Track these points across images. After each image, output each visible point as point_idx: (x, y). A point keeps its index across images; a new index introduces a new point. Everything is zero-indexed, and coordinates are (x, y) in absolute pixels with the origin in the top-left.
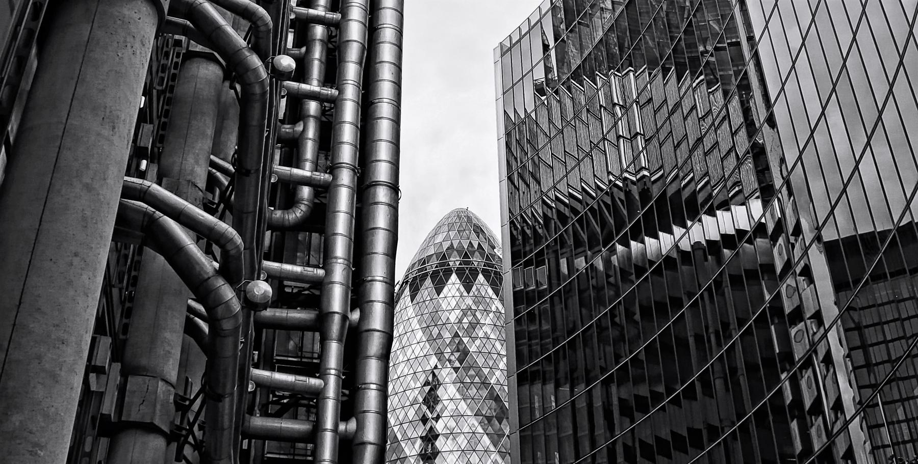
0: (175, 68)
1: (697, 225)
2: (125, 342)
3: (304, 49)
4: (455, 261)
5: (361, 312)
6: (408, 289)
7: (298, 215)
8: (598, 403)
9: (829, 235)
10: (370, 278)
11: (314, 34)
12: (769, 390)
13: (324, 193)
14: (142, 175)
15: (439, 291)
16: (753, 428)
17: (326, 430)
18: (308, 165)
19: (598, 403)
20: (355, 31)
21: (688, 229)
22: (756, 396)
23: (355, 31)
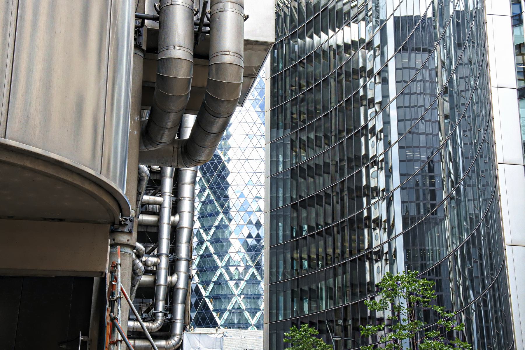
1: (341, 31)
9: (397, 14)
12: (357, 211)
16: (348, 266)
17: (164, 223)
21: (336, 33)
22: (351, 211)
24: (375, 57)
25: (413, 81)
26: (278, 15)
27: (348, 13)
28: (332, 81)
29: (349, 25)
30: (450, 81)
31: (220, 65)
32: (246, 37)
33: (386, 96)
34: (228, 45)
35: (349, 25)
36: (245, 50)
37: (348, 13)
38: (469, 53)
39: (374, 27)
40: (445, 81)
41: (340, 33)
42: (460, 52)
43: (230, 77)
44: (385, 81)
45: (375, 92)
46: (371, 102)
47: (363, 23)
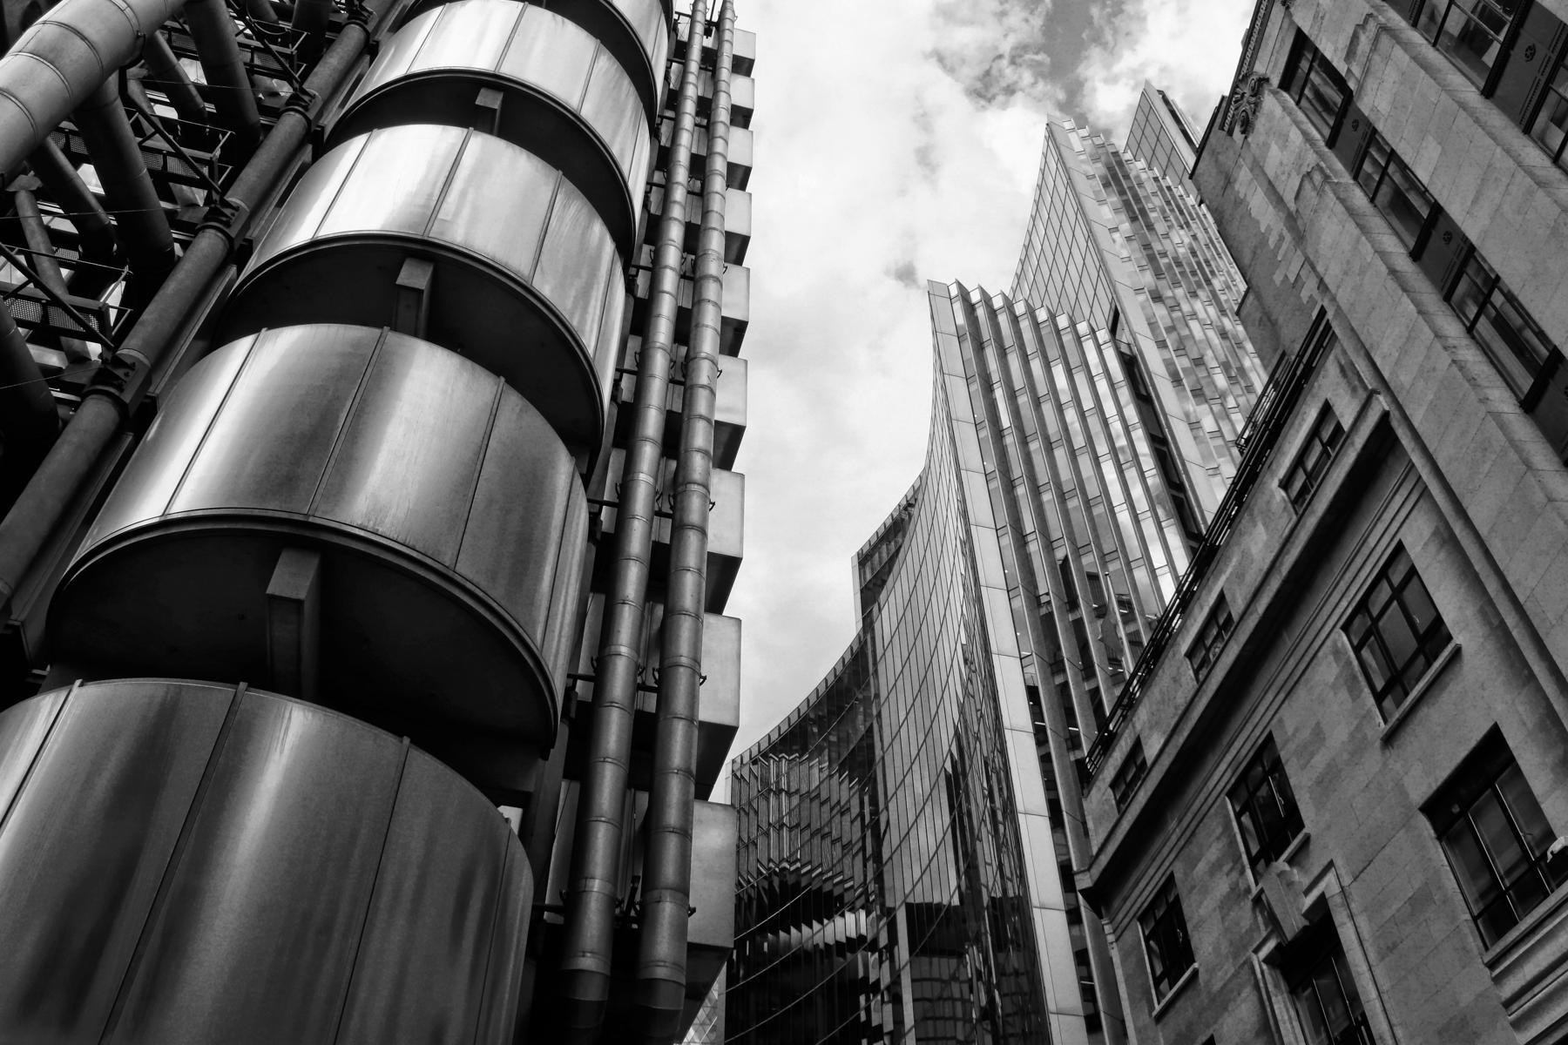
24: (881, 962)
25: (940, 998)
26: (738, 897)
27: (841, 897)
28: (819, 1000)
29: (843, 915)
30: (991, 1000)
31: (652, 983)
32: (690, 939)
33: (899, 1020)
34: (664, 947)
35: (843, 915)
36: (689, 957)
37: (841, 897)
38: (1014, 959)
39: (879, 918)
40: (984, 1002)
41: (829, 928)
42: (1001, 956)
43: (666, 1001)
44: (897, 1000)
45: (883, 1016)
46: (875, 988)
47: (863, 914)
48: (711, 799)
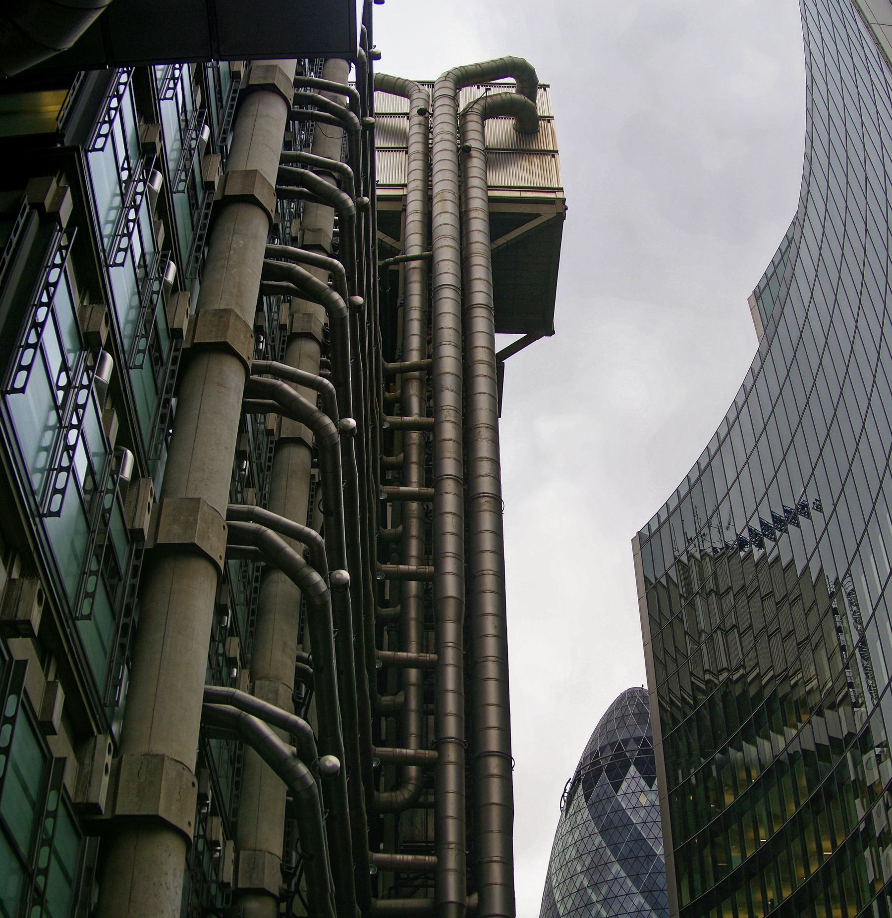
0: (256, 581)
2: (235, 824)
3: (400, 528)
4: (632, 751)
5: (479, 896)
6: (581, 787)
7: (406, 796)
8: (697, 877)
10: (486, 860)
11: (408, 677)
13: (431, 773)
14: (234, 683)
15: (617, 787)
18: (413, 646)
19: (697, 877)
20: (451, 586)
23: (451, 586)
48: (497, 336)
